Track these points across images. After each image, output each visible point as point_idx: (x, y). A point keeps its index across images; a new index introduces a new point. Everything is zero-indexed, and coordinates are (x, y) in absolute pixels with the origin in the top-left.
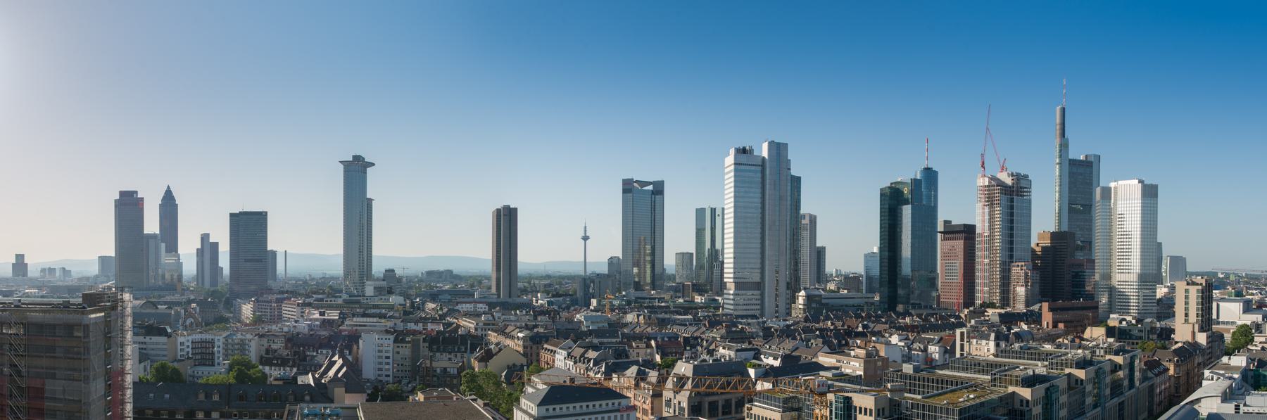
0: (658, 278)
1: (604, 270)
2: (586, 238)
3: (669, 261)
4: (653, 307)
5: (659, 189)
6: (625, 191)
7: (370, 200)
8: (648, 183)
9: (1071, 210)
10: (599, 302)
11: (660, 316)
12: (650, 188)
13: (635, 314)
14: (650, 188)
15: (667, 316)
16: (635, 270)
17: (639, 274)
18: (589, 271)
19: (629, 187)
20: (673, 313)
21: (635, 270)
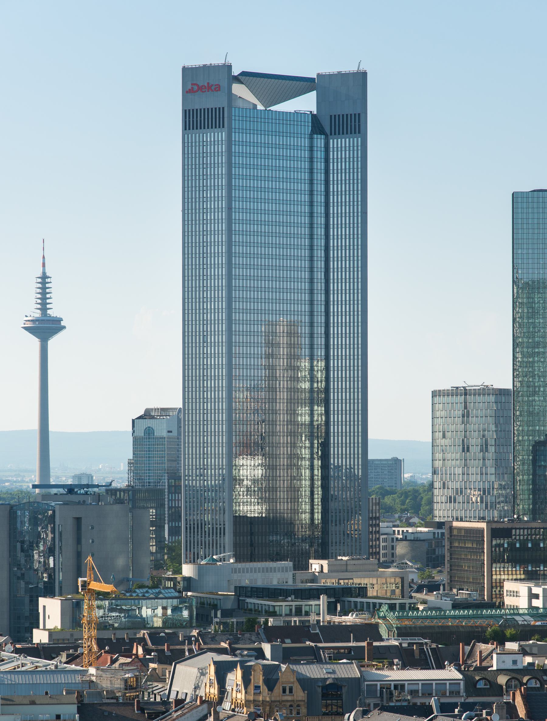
0: (356, 502)
1: (113, 467)
2: (45, 328)
3: (400, 424)
4: (303, 632)
5: (342, 110)
6: (195, 120)
7: (318, 75)
8: (299, 85)
9: (262, 597)
10: (73, 614)
11: (314, 671)
12: (307, 103)
13: (208, 660)
14: (307, 103)
15: (348, 670)
16: (250, 468)
17: (266, 489)
18: (62, 473)
19: (208, 101)
20: (384, 656)
21: (250, 468)
